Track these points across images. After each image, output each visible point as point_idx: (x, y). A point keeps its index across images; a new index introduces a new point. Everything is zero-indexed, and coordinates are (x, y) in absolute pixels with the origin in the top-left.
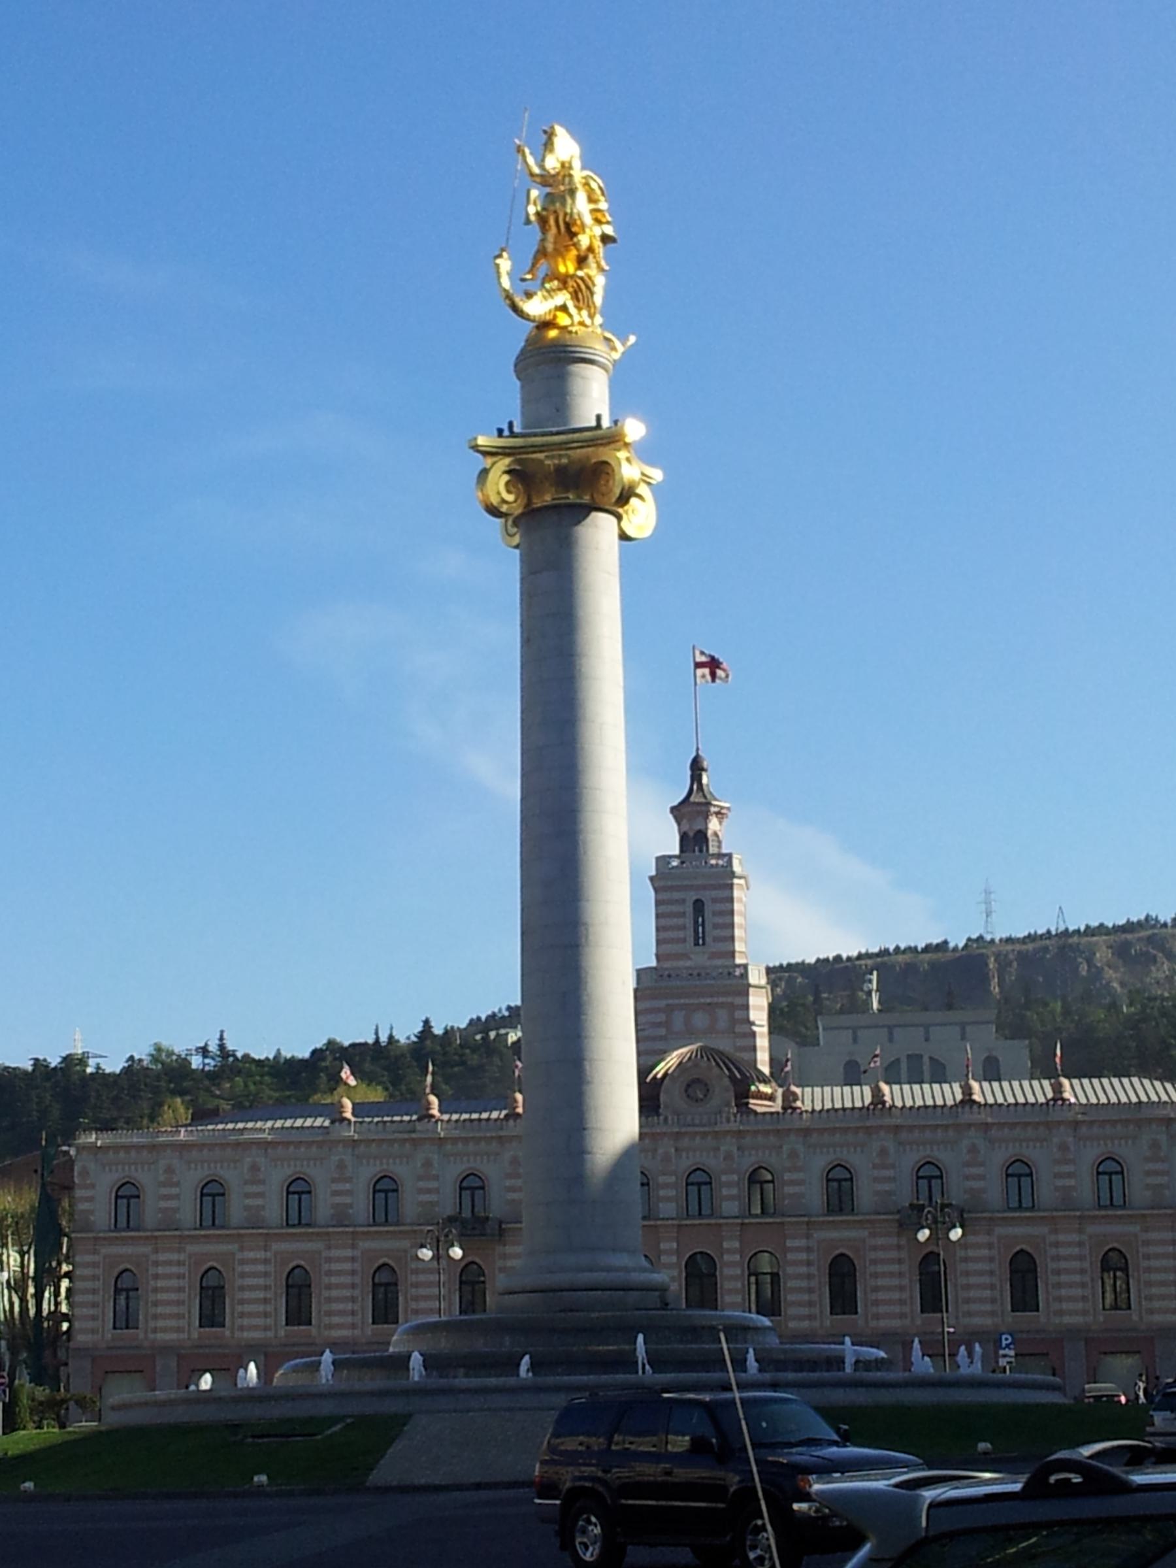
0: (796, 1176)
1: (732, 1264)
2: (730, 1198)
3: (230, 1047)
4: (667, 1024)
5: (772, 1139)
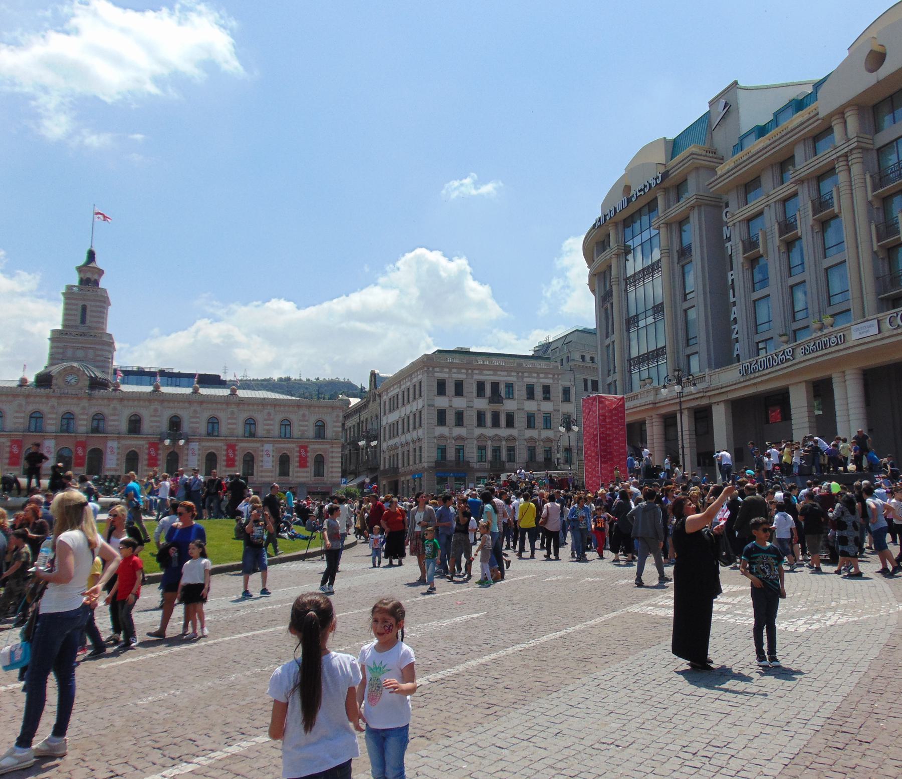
0: (114, 418)
5: (105, 402)
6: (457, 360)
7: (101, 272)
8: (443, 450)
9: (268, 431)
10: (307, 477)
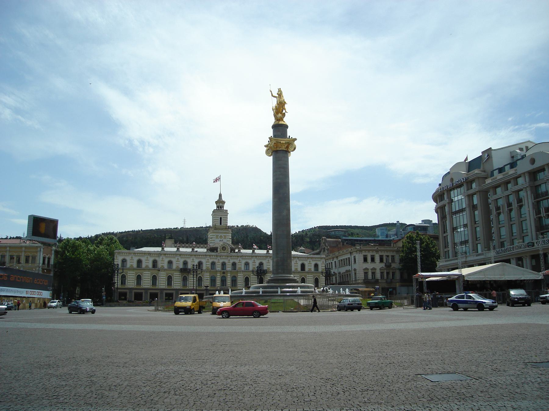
2: (229, 268)
6: (360, 230)
7: (224, 202)
8: (366, 274)
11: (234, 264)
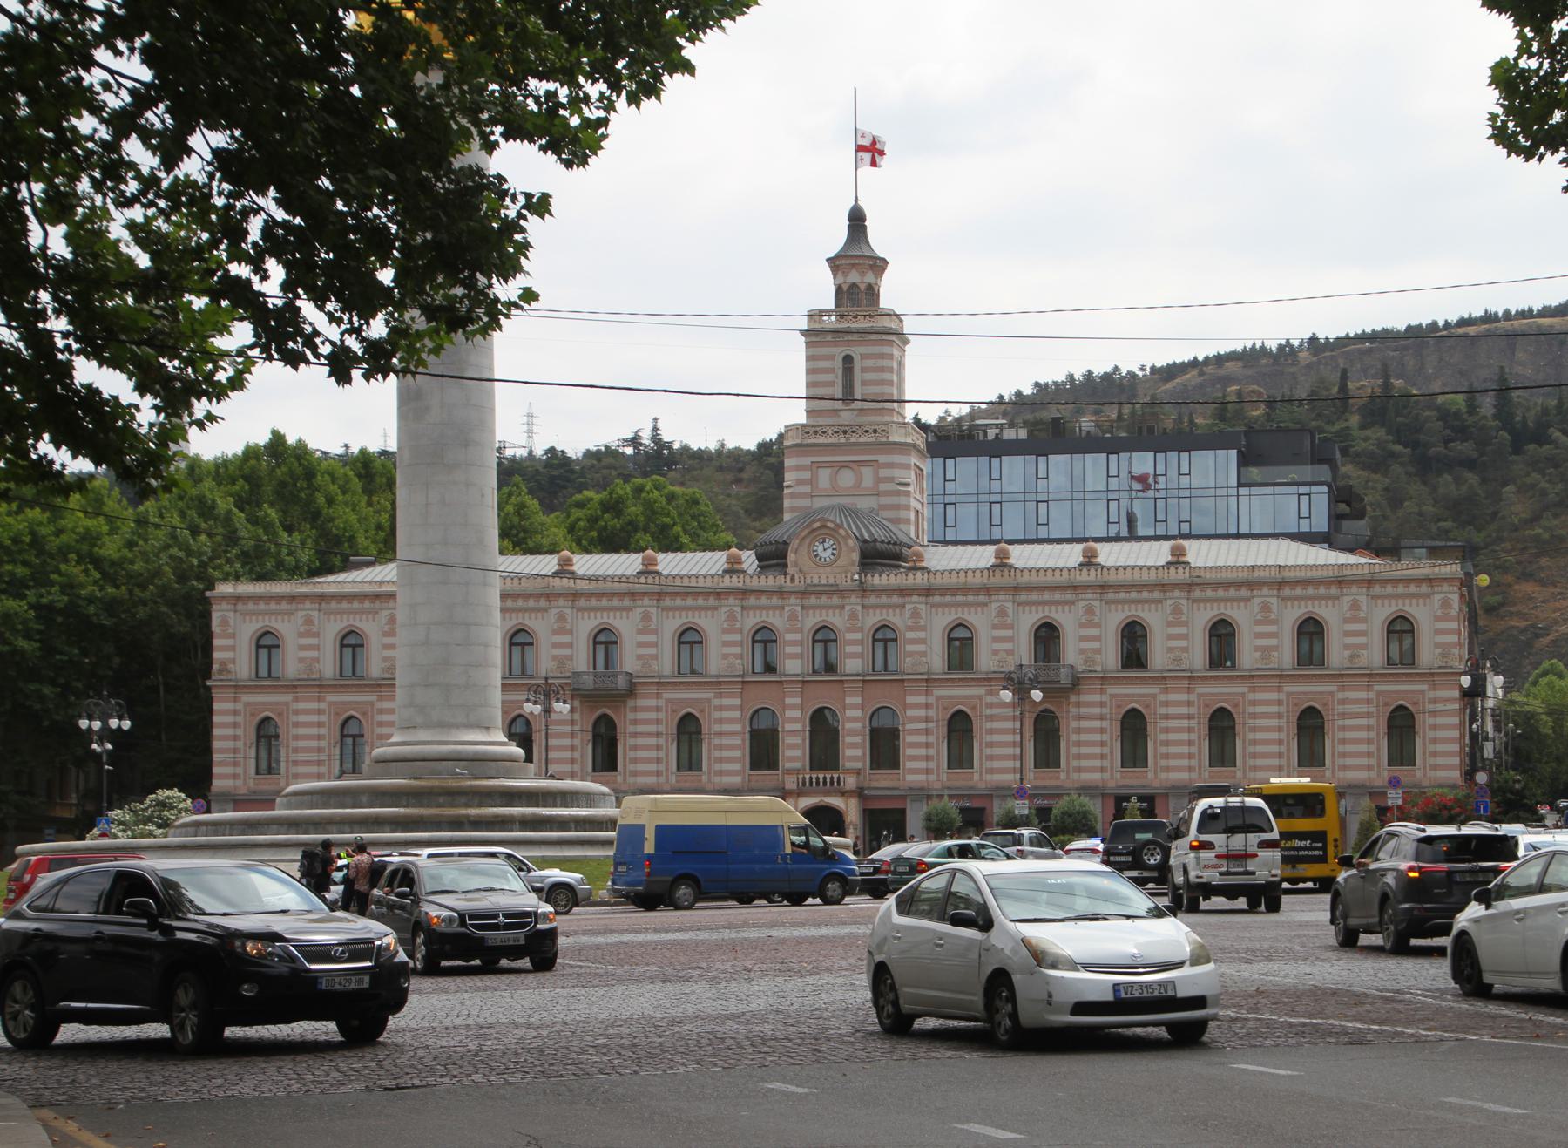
1: (793, 720)
3: (666, 438)
4: (812, 482)
7: (879, 265)
9: (1266, 652)
10: (928, 771)
11: (884, 637)
